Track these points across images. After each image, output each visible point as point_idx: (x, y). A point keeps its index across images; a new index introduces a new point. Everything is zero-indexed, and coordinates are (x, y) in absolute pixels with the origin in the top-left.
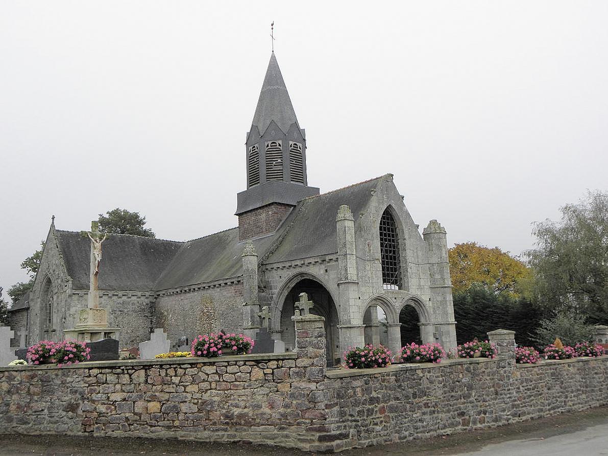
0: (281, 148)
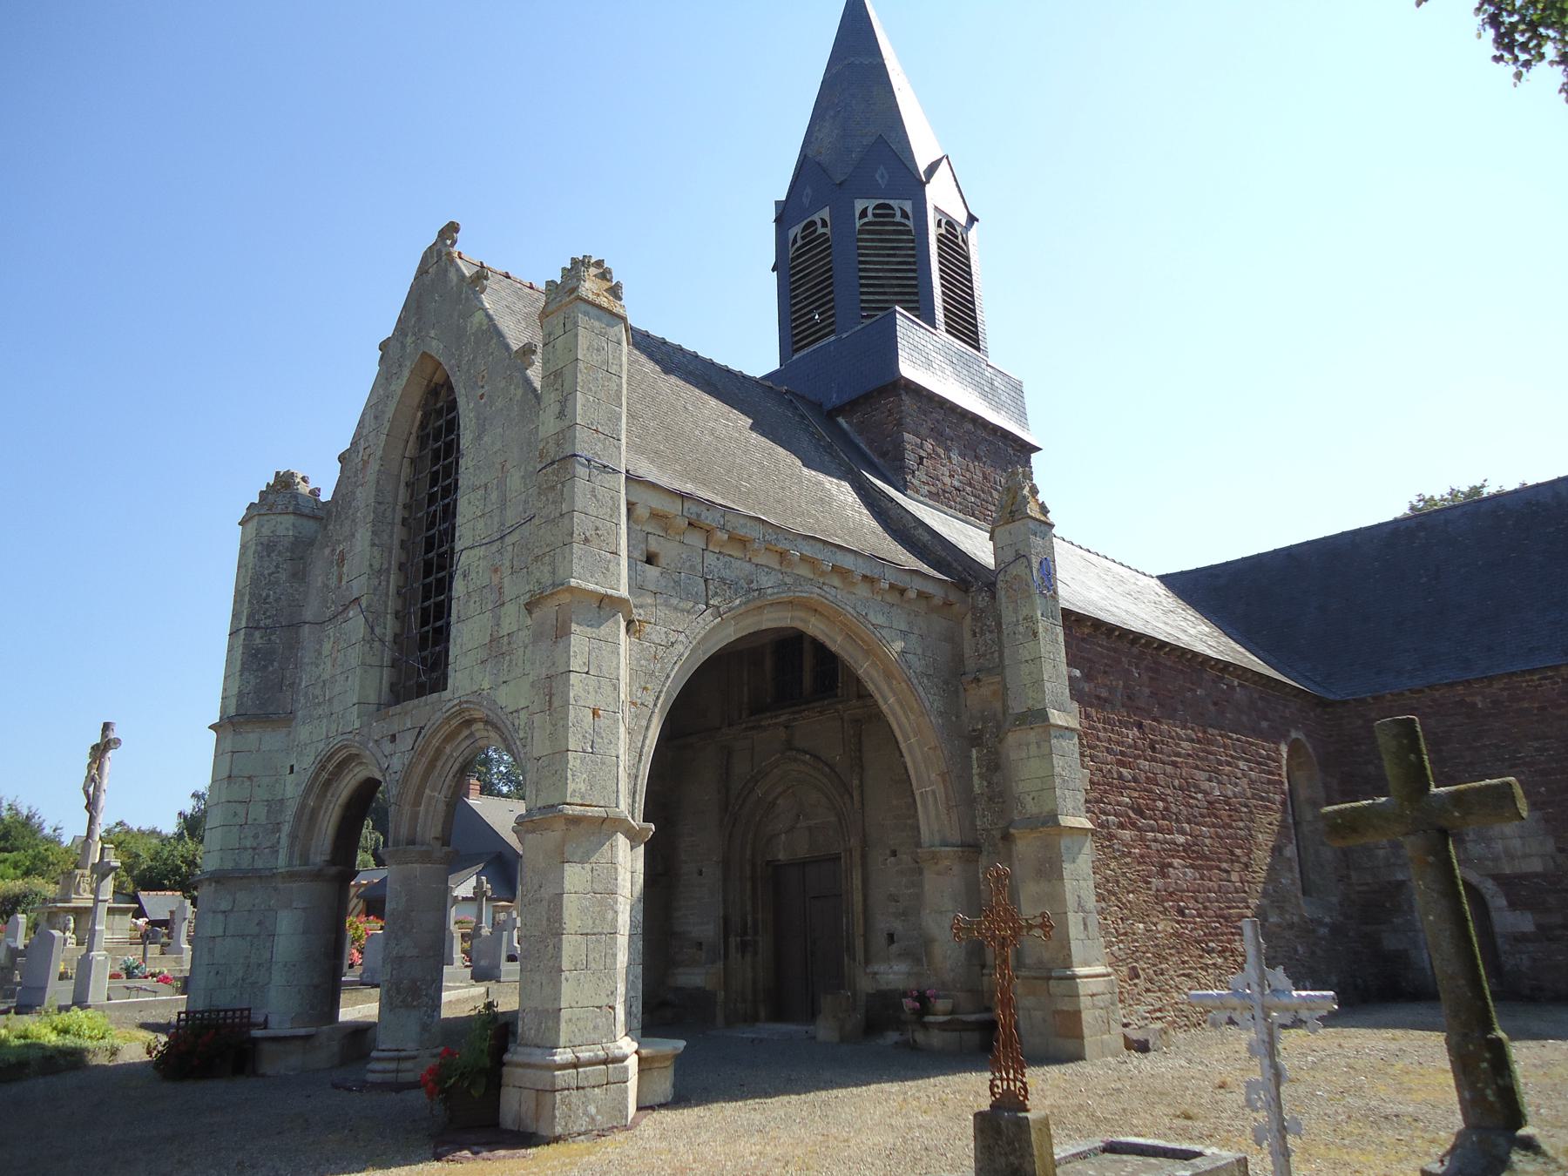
0: (910, 224)
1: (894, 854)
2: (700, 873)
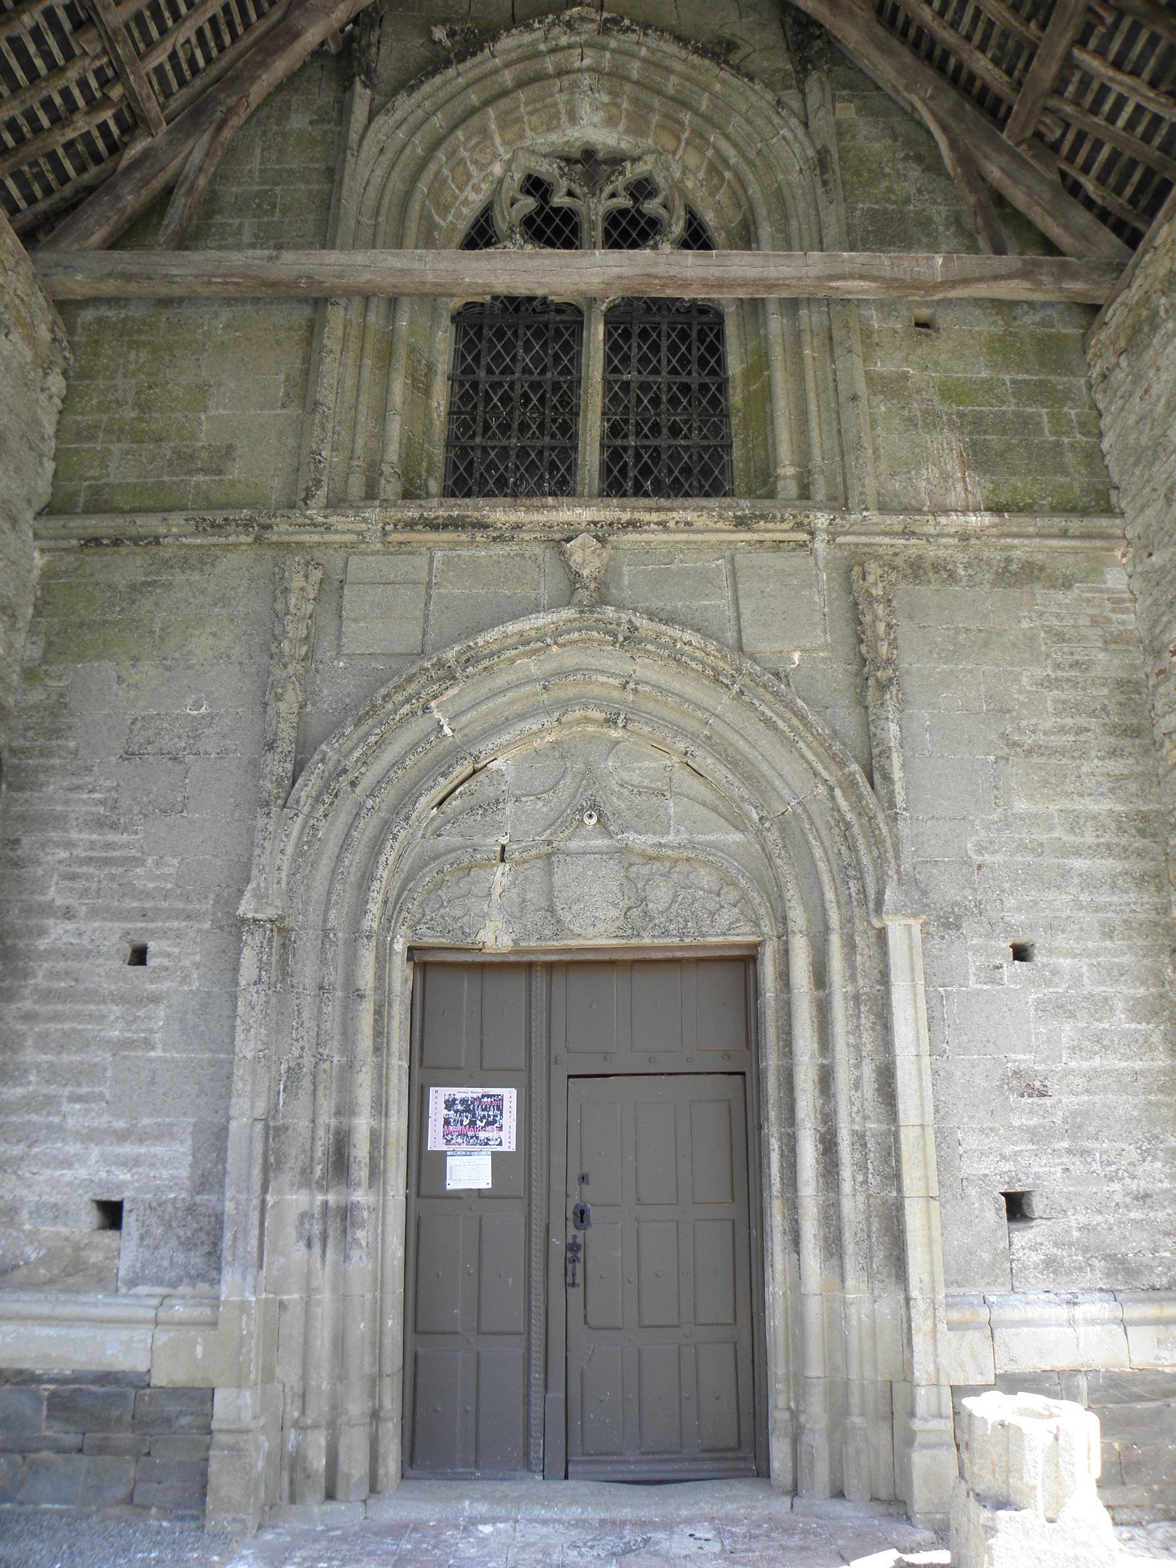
1: (1021, 953)
2: (139, 956)
